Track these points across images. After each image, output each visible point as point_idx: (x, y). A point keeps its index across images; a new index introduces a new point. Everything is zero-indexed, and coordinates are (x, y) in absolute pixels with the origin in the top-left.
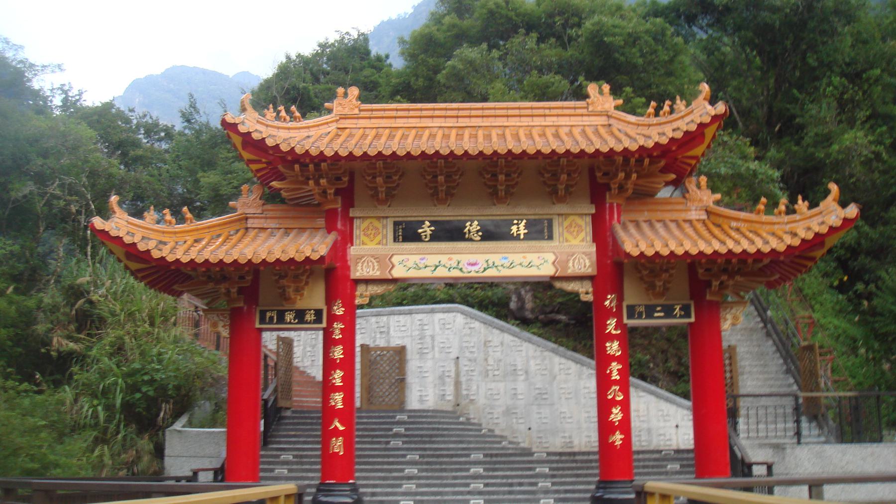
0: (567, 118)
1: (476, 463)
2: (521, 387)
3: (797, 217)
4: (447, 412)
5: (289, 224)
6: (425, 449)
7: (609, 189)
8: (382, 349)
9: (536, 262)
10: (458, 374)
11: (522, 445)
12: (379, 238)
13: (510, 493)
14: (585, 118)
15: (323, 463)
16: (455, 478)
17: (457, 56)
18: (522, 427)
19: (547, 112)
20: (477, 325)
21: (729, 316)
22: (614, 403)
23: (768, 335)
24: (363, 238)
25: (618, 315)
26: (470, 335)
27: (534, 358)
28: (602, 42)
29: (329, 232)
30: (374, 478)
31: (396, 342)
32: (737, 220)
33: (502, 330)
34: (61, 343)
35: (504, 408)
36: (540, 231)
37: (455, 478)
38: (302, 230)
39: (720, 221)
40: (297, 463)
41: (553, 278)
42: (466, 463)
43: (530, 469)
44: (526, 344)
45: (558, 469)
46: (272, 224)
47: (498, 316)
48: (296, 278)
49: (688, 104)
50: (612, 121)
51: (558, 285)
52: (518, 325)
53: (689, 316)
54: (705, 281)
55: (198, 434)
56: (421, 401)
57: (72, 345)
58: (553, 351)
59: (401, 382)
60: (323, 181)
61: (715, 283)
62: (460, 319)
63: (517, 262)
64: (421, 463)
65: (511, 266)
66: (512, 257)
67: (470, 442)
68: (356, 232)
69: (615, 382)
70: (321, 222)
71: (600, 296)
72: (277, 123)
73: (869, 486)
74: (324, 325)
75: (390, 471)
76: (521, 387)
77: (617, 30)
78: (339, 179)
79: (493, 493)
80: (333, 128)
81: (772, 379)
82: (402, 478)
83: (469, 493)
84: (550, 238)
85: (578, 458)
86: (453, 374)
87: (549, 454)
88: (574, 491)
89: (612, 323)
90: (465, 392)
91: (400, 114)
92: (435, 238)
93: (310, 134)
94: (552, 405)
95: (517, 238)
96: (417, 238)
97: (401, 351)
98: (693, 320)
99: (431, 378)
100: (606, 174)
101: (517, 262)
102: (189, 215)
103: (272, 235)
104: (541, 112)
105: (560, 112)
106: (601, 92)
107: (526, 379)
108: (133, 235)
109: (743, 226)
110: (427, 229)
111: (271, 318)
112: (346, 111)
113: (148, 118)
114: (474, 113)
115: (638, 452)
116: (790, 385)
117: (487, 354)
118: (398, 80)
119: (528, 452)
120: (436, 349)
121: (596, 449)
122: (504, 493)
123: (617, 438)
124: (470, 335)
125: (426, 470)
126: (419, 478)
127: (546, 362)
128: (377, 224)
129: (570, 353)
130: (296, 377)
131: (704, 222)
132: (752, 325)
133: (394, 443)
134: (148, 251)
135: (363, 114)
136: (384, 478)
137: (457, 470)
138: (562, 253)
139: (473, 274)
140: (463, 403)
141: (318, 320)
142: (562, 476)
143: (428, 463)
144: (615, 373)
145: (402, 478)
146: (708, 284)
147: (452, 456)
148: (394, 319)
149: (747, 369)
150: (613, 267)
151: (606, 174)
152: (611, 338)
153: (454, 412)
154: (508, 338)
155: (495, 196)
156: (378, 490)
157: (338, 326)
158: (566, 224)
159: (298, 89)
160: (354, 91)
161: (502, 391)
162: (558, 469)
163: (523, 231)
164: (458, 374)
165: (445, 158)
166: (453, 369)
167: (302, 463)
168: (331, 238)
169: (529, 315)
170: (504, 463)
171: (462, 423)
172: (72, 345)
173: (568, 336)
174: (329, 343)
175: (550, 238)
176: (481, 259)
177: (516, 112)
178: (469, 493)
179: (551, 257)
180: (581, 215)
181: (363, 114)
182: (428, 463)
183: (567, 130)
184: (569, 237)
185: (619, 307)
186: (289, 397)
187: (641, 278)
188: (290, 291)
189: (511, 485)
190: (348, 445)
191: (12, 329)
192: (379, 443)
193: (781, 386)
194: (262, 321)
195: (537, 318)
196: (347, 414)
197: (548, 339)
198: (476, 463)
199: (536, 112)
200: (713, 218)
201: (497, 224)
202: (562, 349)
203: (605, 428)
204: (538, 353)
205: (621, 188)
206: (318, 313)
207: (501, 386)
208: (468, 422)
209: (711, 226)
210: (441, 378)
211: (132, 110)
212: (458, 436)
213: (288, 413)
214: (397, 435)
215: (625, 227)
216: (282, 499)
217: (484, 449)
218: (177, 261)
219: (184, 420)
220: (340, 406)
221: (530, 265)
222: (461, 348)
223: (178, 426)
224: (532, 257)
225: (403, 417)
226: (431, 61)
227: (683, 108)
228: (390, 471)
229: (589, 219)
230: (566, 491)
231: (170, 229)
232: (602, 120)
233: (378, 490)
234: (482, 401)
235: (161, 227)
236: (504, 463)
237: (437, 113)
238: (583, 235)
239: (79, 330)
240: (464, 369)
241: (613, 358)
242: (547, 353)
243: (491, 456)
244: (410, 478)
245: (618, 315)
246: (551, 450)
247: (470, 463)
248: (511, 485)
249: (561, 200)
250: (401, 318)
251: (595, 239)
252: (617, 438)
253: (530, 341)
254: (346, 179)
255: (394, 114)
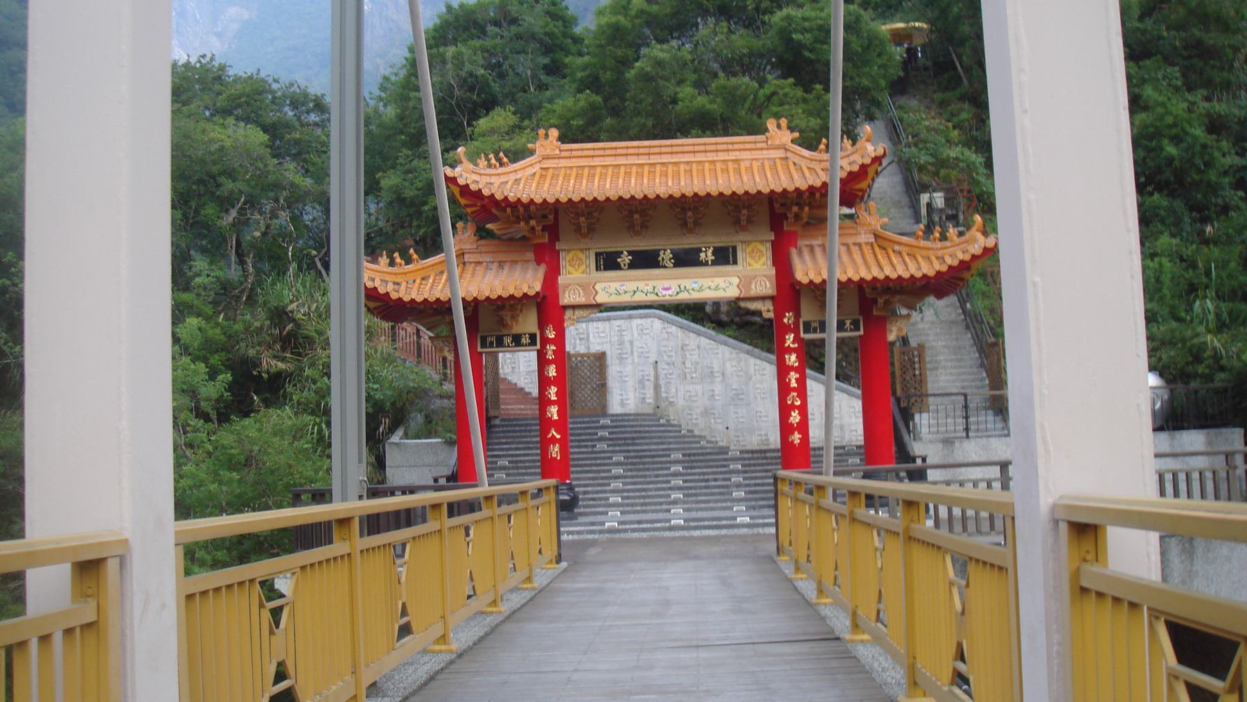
0: (748, 153)
1: (676, 462)
2: (718, 388)
3: (947, 244)
4: (648, 415)
5: (503, 257)
6: (629, 451)
7: (787, 218)
8: (582, 355)
9: (722, 285)
10: (657, 377)
11: (720, 444)
12: (584, 267)
13: (706, 487)
14: (765, 152)
15: (542, 467)
16: (657, 476)
17: (645, 56)
18: (721, 427)
19: (730, 147)
20: (674, 329)
21: (894, 329)
22: (793, 407)
23: (967, 327)
24: (569, 268)
25: (796, 331)
26: (667, 340)
27: (730, 360)
28: (790, 40)
29: (538, 264)
30: (584, 479)
31: (595, 348)
32: (899, 243)
33: (698, 334)
34: (271, 363)
35: (702, 409)
36: (725, 256)
37: (657, 476)
38: (514, 262)
39: (885, 244)
40: (513, 468)
41: (738, 299)
42: (666, 462)
43: (724, 466)
44: (722, 347)
45: (750, 465)
46: (488, 258)
47: (695, 320)
48: (512, 308)
49: (854, 144)
50: (789, 155)
51: (742, 304)
52: (714, 329)
53: (859, 330)
54: (872, 302)
55: (417, 445)
56: (622, 404)
57: (281, 365)
58: (748, 353)
59: (603, 387)
60: (533, 223)
61: (881, 301)
62: (657, 324)
63: (706, 285)
64: (626, 464)
65: (701, 289)
66: (701, 282)
67: (670, 443)
68: (562, 263)
69: (794, 389)
70: (531, 256)
71: (779, 314)
72: (489, 171)
73: (978, 469)
74: (538, 347)
75: (599, 472)
76: (718, 388)
77: (807, 24)
78: (545, 217)
79: (691, 488)
80: (537, 168)
81: (964, 373)
82: (610, 478)
83: (670, 489)
84: (735, 262)
85: (768, 455)
86: (652, 378)
87: (741, 452)
88: (763, 485)
89: (790, 338)
90: (664, 395)
91: (597, 153)
92: (632, 266)
93: (518, 176)
94: (748, 404)
95: (706, 264)
96: (617, 267)
97: (601, 357)
98: (862, 332)
99: (631, 382)
100: (783, 205)
101: (706, 285)
102: (415, 256)
103: (487, 268)
104: (725, 147)
105: (741, 146)
106: (779, 127)
107: (723, 380)
108: (373, 280)
109: (904, 249)
110: (625, 259)
111: (491, 343)
112: (548, 152)
113: (295, 88)
114: (664, 150)
115: (815, 449)
116: (982, 380)
117: (684, 357)
118: (584, 74)
119: (724, 450)
120: (636, 354)
121: (779, 446)
122: (701, 488)
123: (796, 438)
124: (667, 340)
125: (631, 470)
126: (625, 477)
127: (742, 363)
128: (582, 256)
129: (765, 354)
130: (502, 386)
131: (872, 245)
132: (953, 316)
133: (602, 446)
134: (387, 293)
135: (563, 154)
136: (593, 479)
137: (658, 469)
138: (746, 277)
139: (668, 298)
140: (663, 405)
141: (533, 343)
142: (753, 472)
143: (632, 464)
144: (793, 381)
145: (610, 478)
146: (875, 301)
147: (654, 456)
148: (593, 326)
149: (943, 363)
150: (790, 293)
151: (783, 205)
152: (790, 350)
153: (655, 414)
154: (704, 341)
155: (686, 227)
156: (590, 489)
157: (551, 348)
158: (749, 249)
159: (476, 77)
160: (554, 133)
161: (700, 393)
162: (750, 465)
163: (711, 257)
164: (657, 377)
165: (640, 201)
166: (652, 373)
167: (518, 468)
168: (542, 270)
169: (724, 318)
170: (701, 461)
171: (663, 425)
172: (281, 365)
173: (762, 337)
174: (542, 362)
175: (735, 262)
176: (674, 284)
177: (702, 148)
178: (670, 489)
179: (736, 281)
180: (762, 242)
181: (563, 154)
182: (632, 464)
183: (747, 164)
184: (752, 262)
185: (796, 323)
186: (497, 406)
187: (816, 297)
188: (508, 320)
189: (707, 481)
190: (564, 450)
191: (223, 354)
192: (586, 446)
193: (973, 380)
194: (483, 346)
195: (732, 321)
196: (561, 425)
197: (743, 341)
198: (676, 462)
199: (720, 147)
200: (880, 241)
201: (686, 251)
202: (756, 350)
203: (786, 429)
204: (734, 356)
205: (797, 217)
206: (533, 337)
207: (699, 388)
208: (669, 424)
209: (877, 248)
210: (641, 382)
211: (276, 81)
212: (660, 437)
213: (497, 422)
214: (602, 439)
215: (800, 253)
216: (78, 630)
217: (683, 449)
218: (413, 300)
219: (400, 432)
220: (555, 417)
221: (717, 288)
222: (659, 353)
223: (395, 438)
224: (719, 281)
225: (607, 421)
226: (619, 53)
227: (849, 147)
228: (599, 472)
229: (769, 245)
230: (756, 485)
231: (401, 271)
232: (781, 153)
233: (590, 489)
234: (681, 402)
235: (395, 269)
236: (701, 461)
237: (630, 151)
238: (764, 259)
239: (283, 349)
240: (662, 373)
241: (792, 368)
242: (742, 355)
243: (689, 455)
244: (616, 477)
245: (796, 331)
246: (749, 447)
247: (670, 462)
248: (707, 481)
249: (743, 229)
250: (600, 324)
251: (774, 263)
252: (796, 438)
253: (726, 344)
254: (551, 217)
255: (591, 153)
